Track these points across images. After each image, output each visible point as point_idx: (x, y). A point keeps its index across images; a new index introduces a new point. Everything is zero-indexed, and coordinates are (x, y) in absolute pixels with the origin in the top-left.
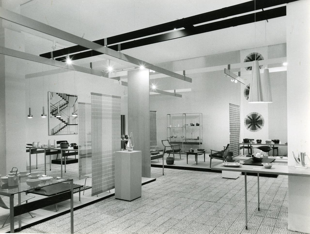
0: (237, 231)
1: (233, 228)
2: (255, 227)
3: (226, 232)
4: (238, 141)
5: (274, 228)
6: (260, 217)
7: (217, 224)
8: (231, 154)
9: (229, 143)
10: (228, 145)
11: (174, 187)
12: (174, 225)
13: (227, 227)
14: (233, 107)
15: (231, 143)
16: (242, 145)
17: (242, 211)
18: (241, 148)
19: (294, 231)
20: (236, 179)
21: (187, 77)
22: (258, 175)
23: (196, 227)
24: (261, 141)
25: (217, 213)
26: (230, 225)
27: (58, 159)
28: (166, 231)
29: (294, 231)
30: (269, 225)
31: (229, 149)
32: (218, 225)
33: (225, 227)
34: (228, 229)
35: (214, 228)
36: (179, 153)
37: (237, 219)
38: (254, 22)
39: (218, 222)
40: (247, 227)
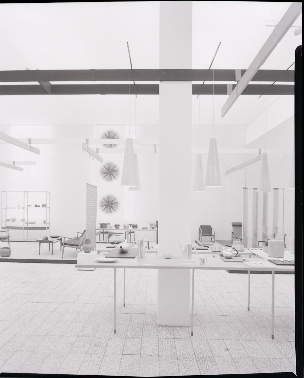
0: (104, 337)
1: (99, 334)
2: (123, 328)
3: (92, 342)
4: (95, 227)
5: (143, 325)
6: (127, 314)
7: (80, 333)
8: (88, 241)
9: (85, 229)
10: (85, 231)
11: (16, 288)
12: (21, 345)
13: (91, 335)
14: (90, 188)
15: (88, 228)
16: (99, 231)
17: (106, 311)
18: (98, 234)
19: (163, 326)
20: (93, 270)
21: (33, 147)
22: (249, 272)
23: (52, 343)
24: (119, 226)
25: (77, 317)
26: (95, 331)
27: (204, 84)
28: (10, 357)
29: (163, 325)
30: (138, 323)
31: (87, 237)
32: (81, 333)
33: (89, 335)
34: (94, 337)
35: (76, 338)
36: (7, 240)
37: (102, 321)
38: (129, 95)
39: (80, 330)
40: (115, 331)
